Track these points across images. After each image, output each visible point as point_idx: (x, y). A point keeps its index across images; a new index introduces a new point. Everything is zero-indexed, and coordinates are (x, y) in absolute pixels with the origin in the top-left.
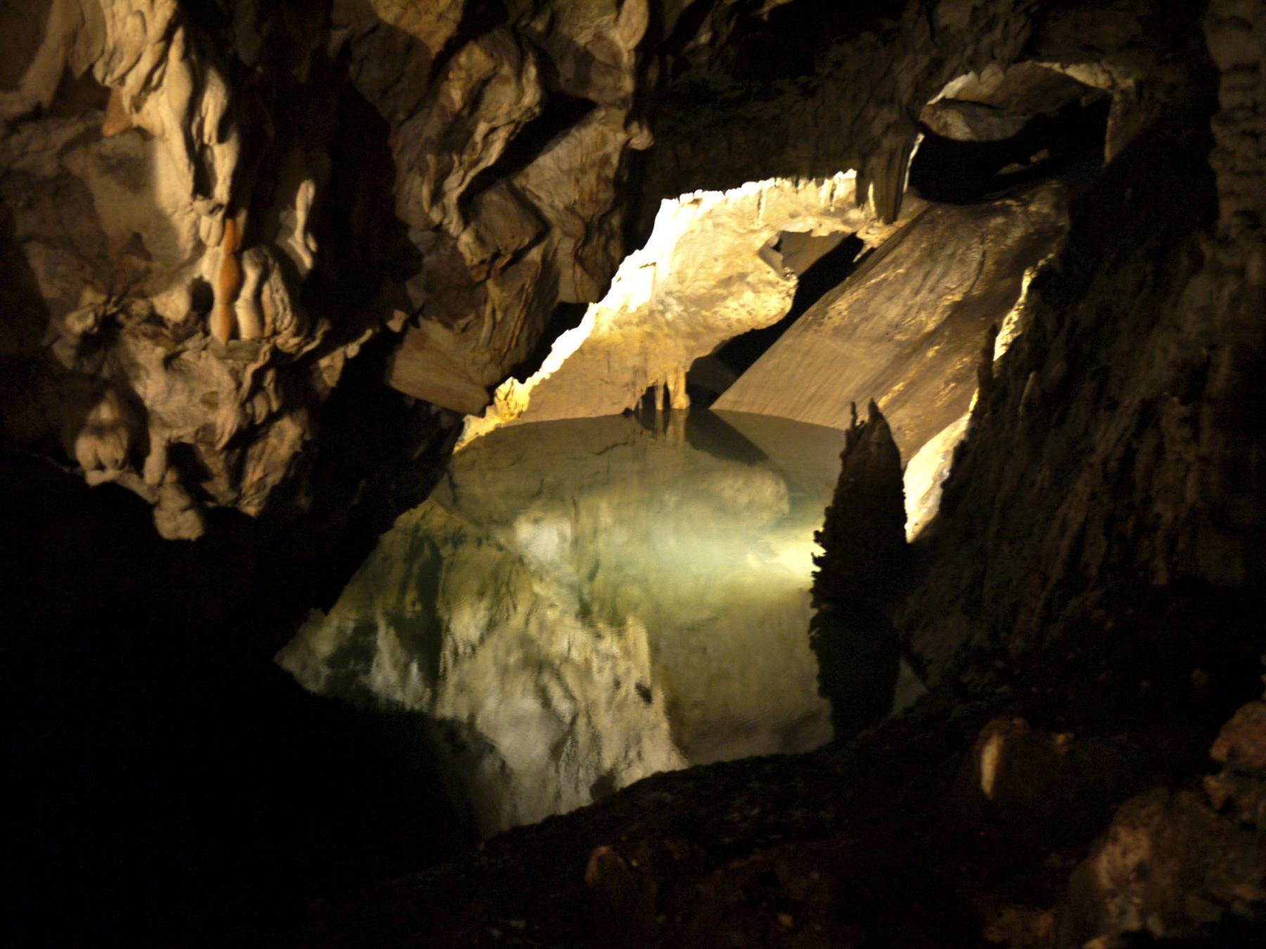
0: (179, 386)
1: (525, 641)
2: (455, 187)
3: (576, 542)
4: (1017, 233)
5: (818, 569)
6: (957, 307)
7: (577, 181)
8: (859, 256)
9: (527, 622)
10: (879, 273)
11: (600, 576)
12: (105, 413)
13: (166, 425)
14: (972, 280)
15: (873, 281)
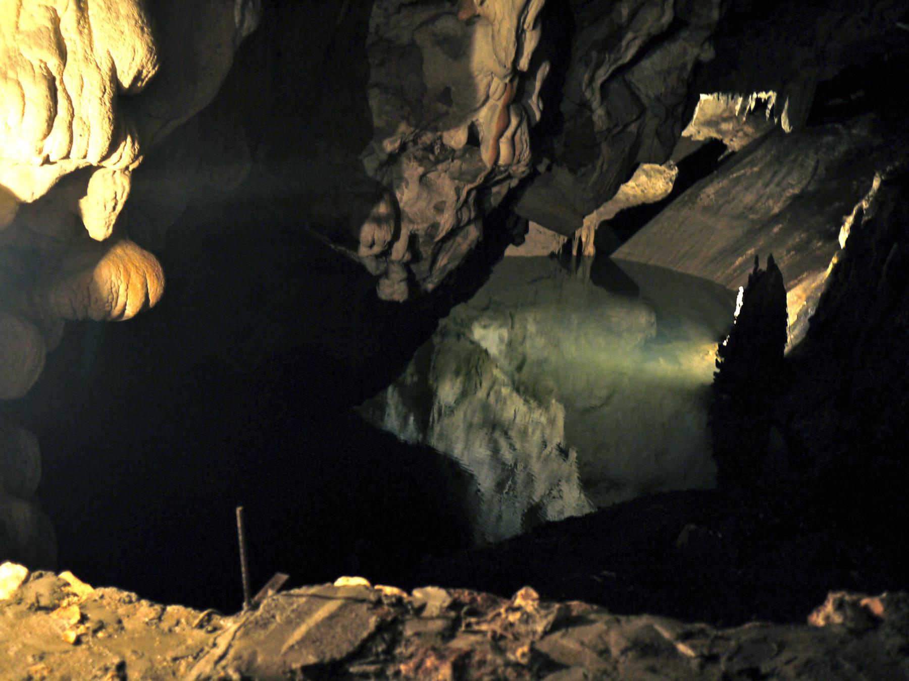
0: (425, 195)
1: (485, 407)
2: (602, 75)
3: (510, 344)
4: (842, 148)
5: (718, 370)
6: (795, 198)
7: (665, 79)
8: (722, 157)
9: (488, 395)
10: (739, 170)
11: (526, 369)
12: (382, 209)
13: (411, 221)
14: (808, 180)
15: (735, 175)
